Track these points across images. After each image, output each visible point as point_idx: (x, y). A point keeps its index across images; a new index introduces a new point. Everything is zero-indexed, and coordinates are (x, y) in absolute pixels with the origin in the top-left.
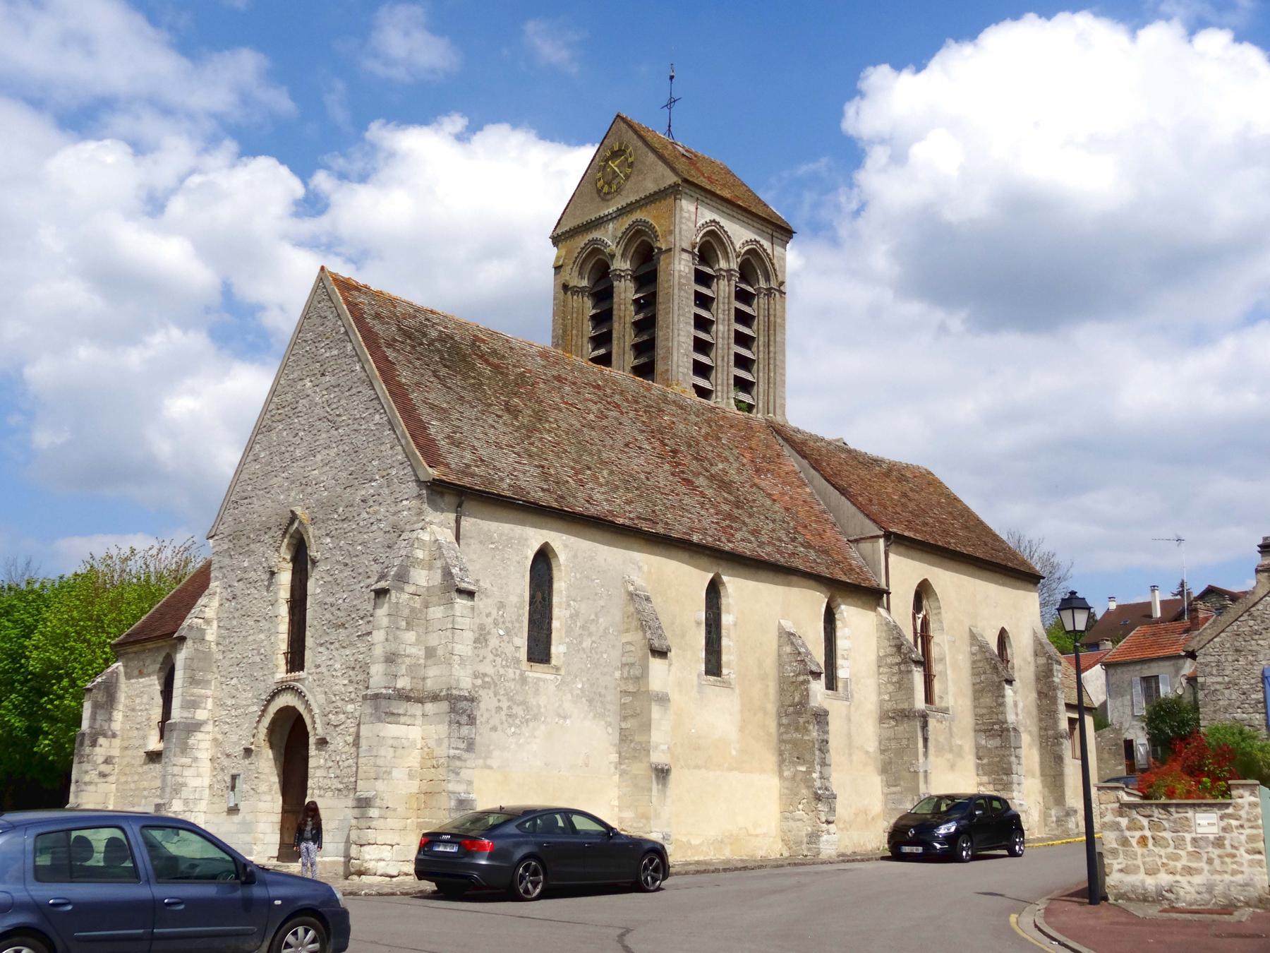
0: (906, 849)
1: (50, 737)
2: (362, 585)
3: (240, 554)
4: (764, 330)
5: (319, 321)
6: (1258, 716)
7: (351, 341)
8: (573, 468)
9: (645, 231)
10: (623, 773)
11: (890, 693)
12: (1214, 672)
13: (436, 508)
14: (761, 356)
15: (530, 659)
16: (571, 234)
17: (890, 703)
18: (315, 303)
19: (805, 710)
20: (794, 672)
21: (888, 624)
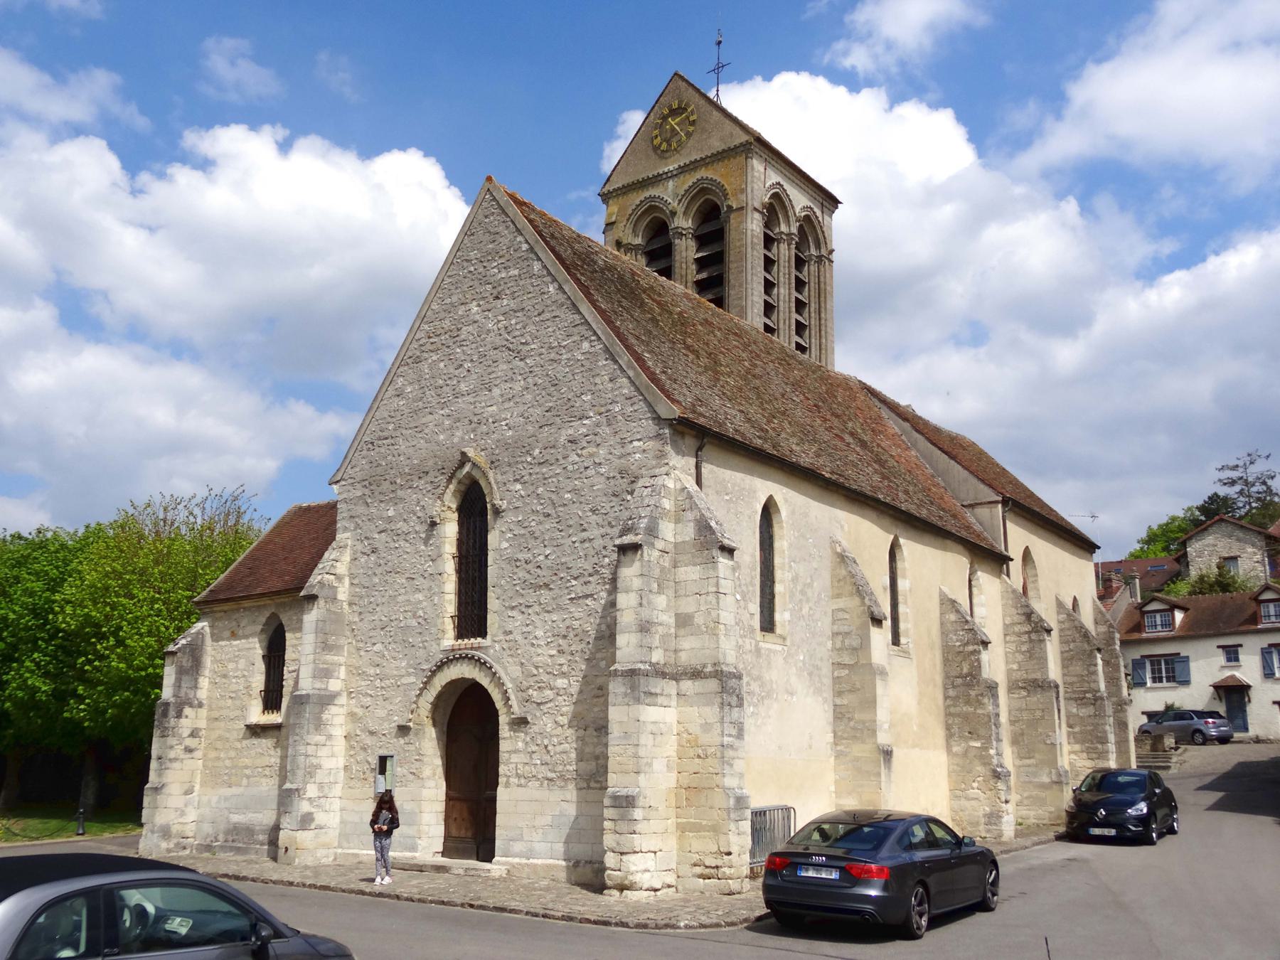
0: (1096, 831)
1: (87, 701)
2: (574, 539)
3: (382, 501)
4: (815, 297)
5: (487, 237)
7: (539, 259)
9: (711, 189)
10: (838, 755)
11: (1018, 663)
13: (679, 452)
14: (813, 323)
15: (763, 629)
16: (624, 190)
18: (480, 217)
19: (978, 682)
20: (961, 641)
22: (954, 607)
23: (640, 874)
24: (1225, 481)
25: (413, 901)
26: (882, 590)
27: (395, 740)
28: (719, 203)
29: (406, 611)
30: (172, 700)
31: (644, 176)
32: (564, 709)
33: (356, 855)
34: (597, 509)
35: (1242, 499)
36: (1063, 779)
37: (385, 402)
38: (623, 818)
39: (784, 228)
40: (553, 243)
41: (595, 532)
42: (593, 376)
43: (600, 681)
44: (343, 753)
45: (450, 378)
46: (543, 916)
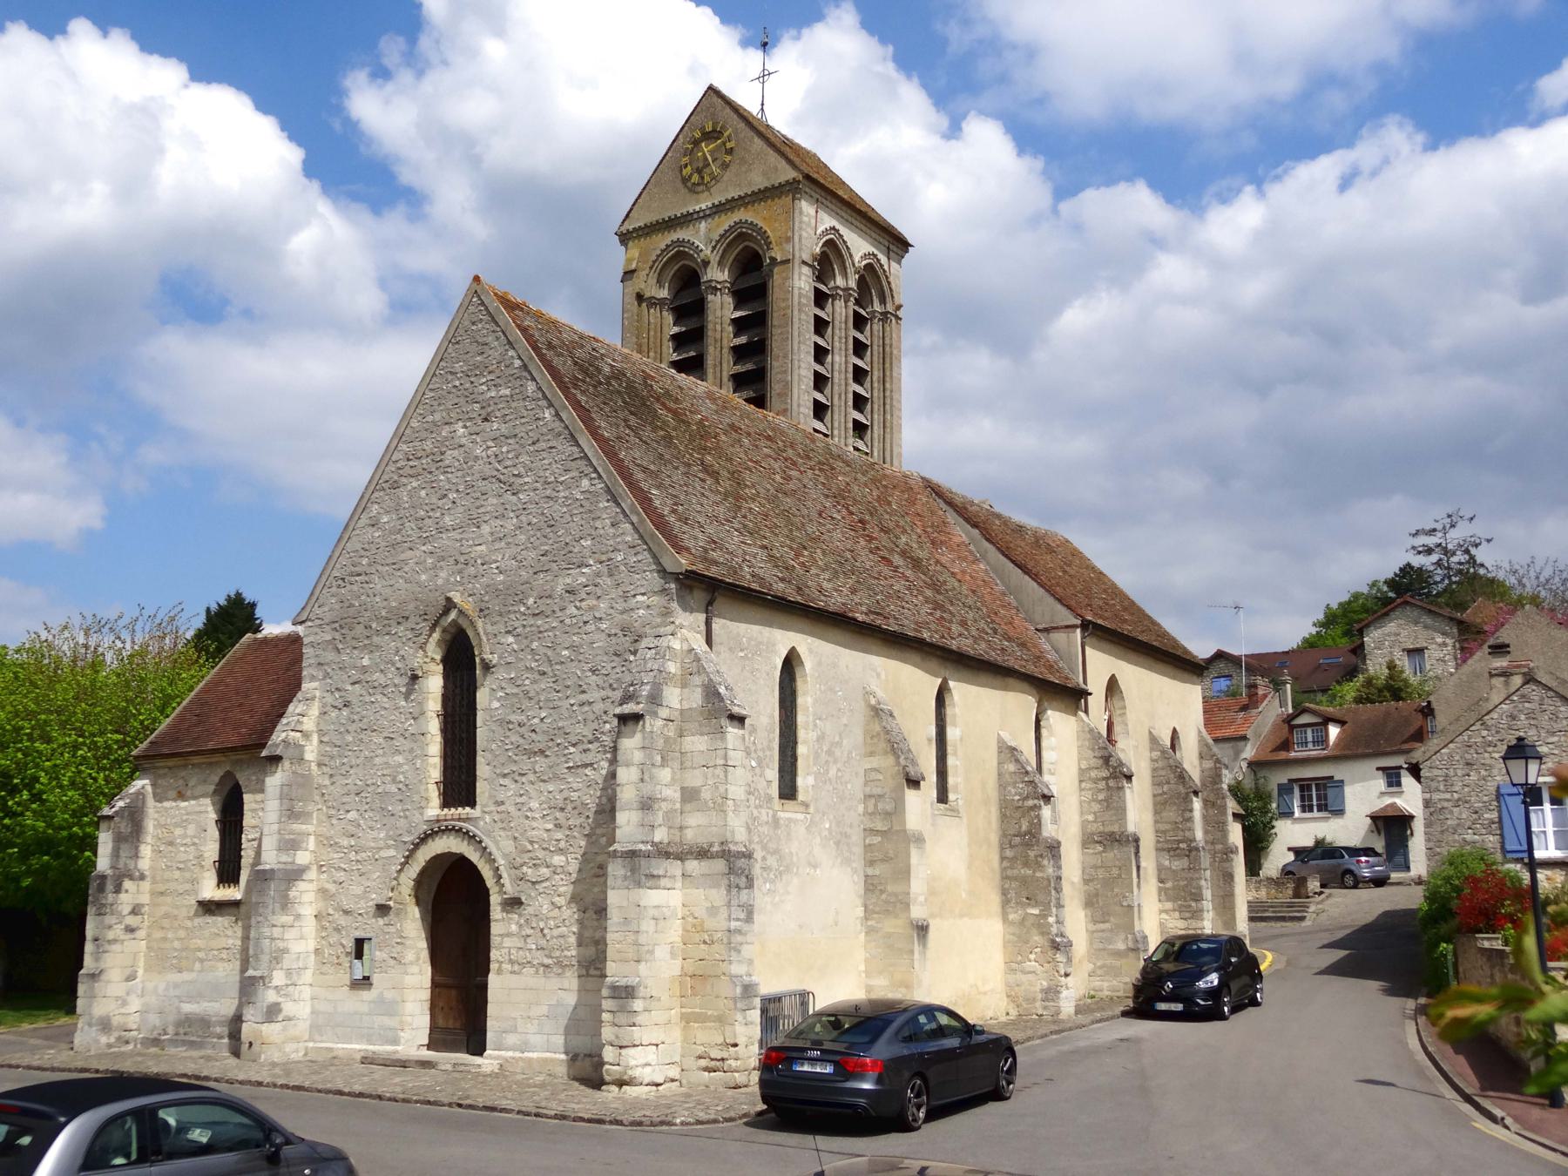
0: (1162, 1006)
2: (572, 702)
3: (355, 648)
6: (1491, 838)
7: (533, 379)
8: (791, 548)
9: (750, 235)
10: (870, 931)
11: (1095, 813)
12: (1442, 788)
13: (687, 608)
14: (875, 394)
15: (782, 796)
16: (646, 231)
17: (1095, 825)
19: (1038, 841)
20: (1020, 794)
21: (1091, 731)
22: (1013, 755)
23: (640, 1069)
24: (1421, 549)
25: (397, 1101)
26: (926, 742)
27: (374, 920)
28: (761, 252)
29: (384, 775)
30: (109, 872)
31: (671, 213)
32: (562, 889)
33: (330, 1049)
34: (597, 670)
35: (1439, 571)
36: (1140, 946)
37: (358, 532)
38: (623, 1009)
39: (840, 281)
40: (549, 354)
41: (594, 695)
42: (593, 519)
43: (600, 859)
44: (313, 934)
45: (433, 510)
46: (535, 1115)
